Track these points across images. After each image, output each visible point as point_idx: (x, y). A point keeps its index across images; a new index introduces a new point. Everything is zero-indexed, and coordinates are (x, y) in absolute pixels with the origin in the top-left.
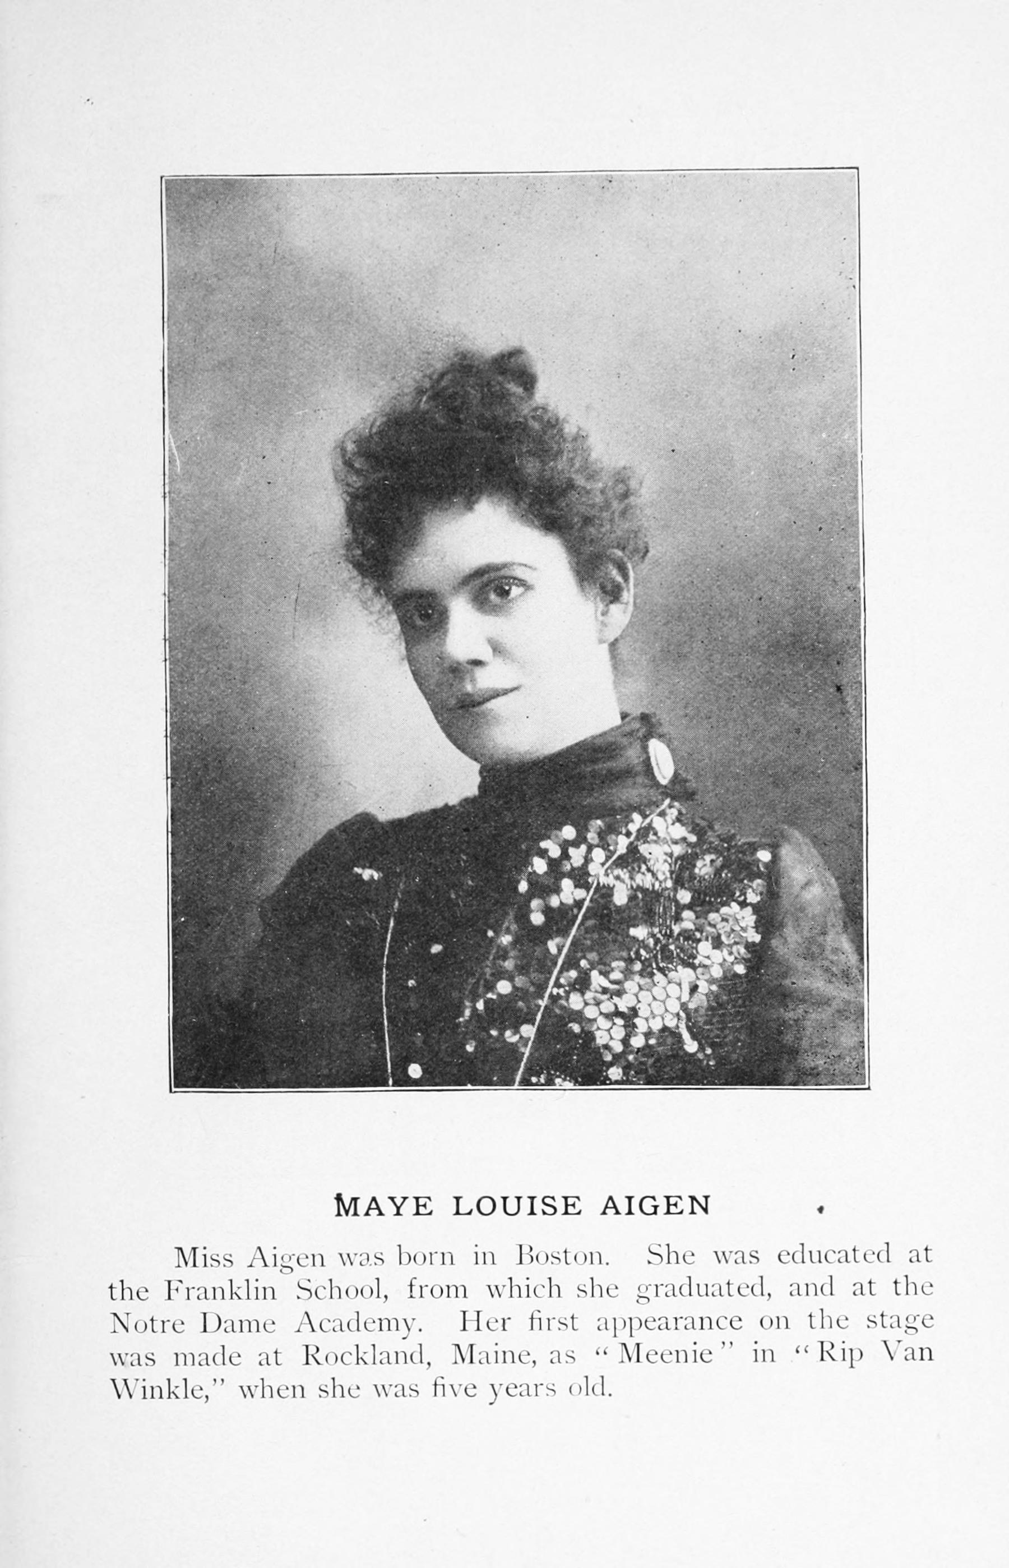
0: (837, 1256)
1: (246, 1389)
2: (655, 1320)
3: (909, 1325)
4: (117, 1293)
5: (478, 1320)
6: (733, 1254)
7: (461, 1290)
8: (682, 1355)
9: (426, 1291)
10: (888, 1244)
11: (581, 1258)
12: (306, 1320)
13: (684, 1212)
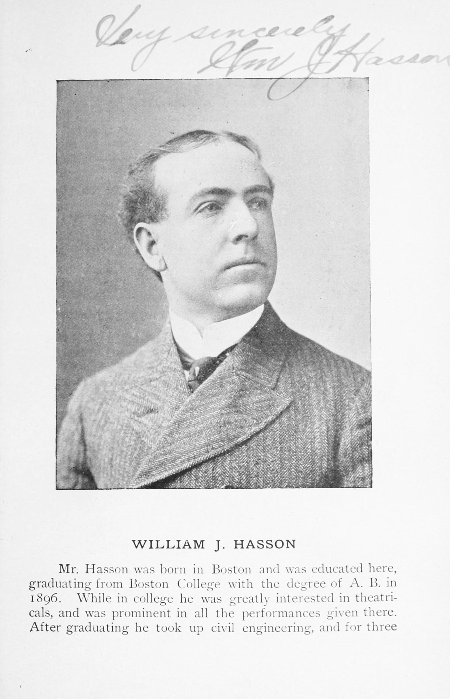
0: (339, 570)
1: (204, 599)
2: (373, 597)
3: (231, 602)
4: (265, 585)
5: (87, 568)
6: (94, 612)
7: (120, 584)
8: (163, 614)
9: (104, 585)
10: (323, 564)
11: (241, 571)
12: (355, 582)
13: (164, 547)
